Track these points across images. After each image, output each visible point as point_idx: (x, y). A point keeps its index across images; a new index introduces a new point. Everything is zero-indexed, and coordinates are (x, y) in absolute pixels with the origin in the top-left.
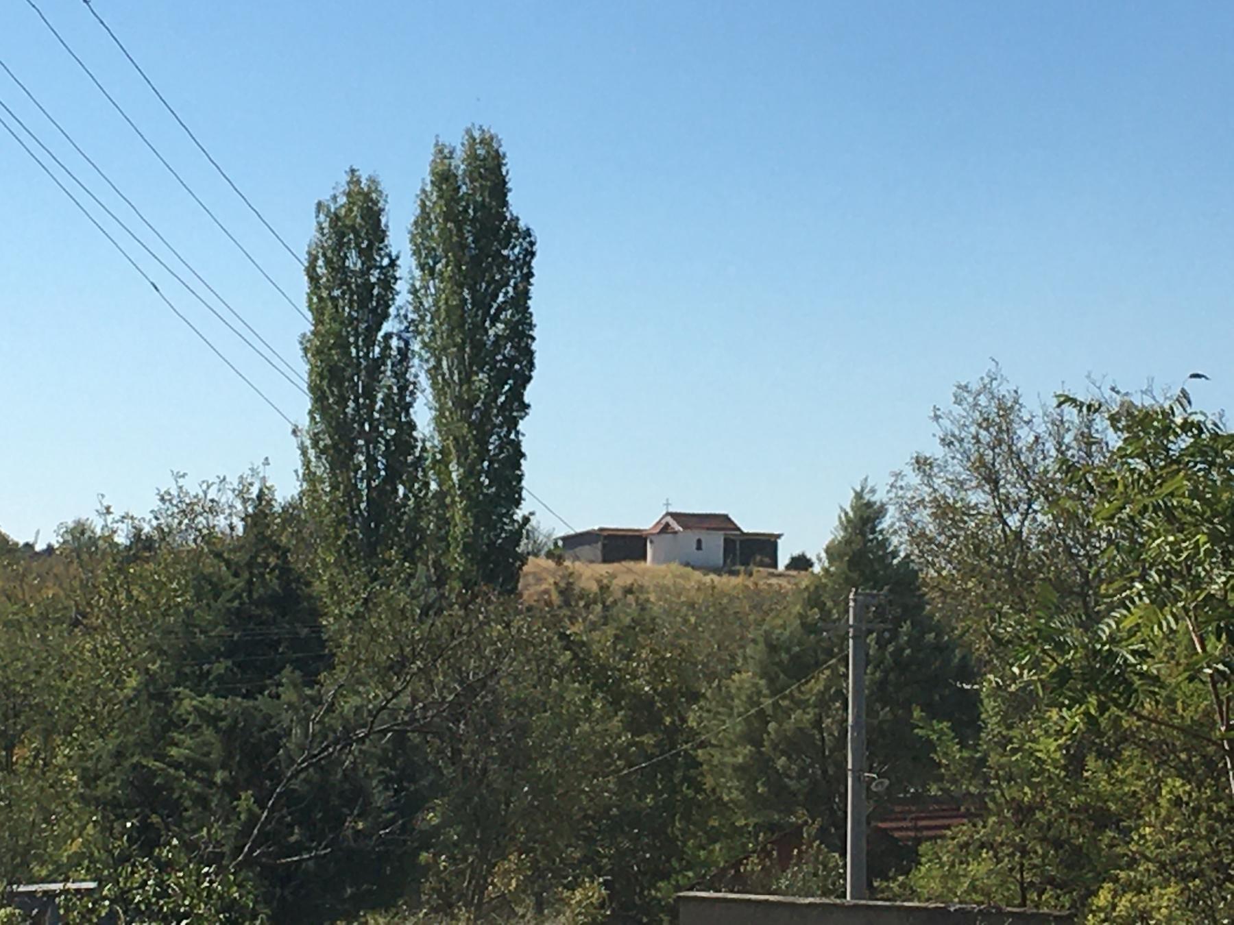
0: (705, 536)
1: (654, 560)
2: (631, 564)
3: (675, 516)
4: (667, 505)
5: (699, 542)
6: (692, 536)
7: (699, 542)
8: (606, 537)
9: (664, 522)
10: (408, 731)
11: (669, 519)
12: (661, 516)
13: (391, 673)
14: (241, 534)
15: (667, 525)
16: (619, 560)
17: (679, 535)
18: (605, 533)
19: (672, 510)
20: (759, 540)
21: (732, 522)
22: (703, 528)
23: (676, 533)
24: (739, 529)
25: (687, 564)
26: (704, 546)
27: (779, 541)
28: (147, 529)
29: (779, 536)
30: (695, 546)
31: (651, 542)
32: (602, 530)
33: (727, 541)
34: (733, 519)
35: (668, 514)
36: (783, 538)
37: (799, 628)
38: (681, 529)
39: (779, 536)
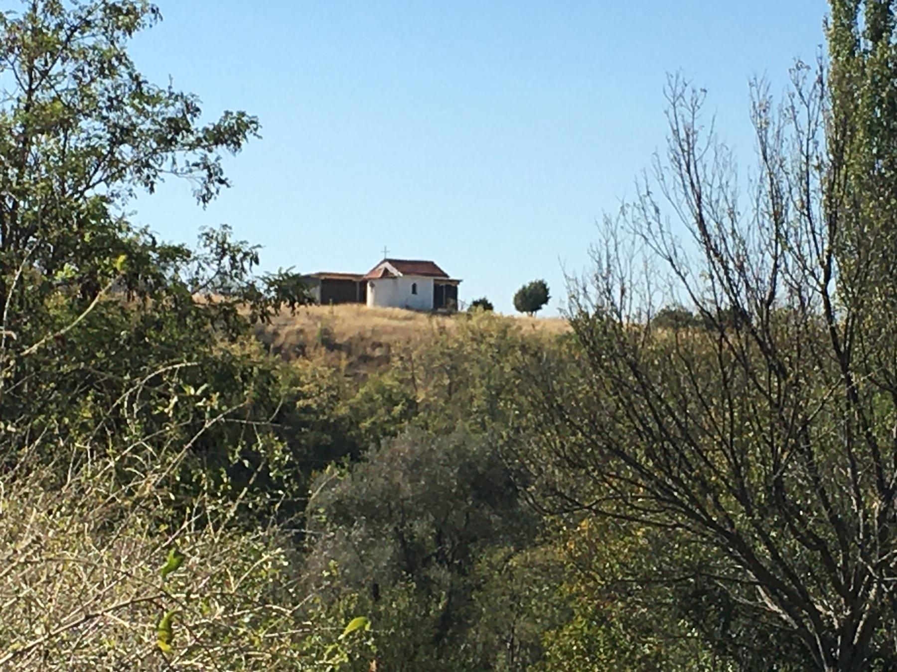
0: (419, 280)
1: (376, 302)
2: (355, 306)
3: (395, 263)
4: (385, 252)
5: (414, 286)
6: (410, 280)
7: (414, 286)
8: (323, 281)
9: (383, 266)
10: (465, 661)
11: (387, 265)
12: (378, 262)
13: (374, 520)
14: (282, 303)
15: (386, 271)
16: (336, 302)
17: (399, 280)
18: (323, 278)
19: (389, 257)
20: (350, 281)
21: (439, 269)
22: (419, 274)
23: (395, 278)
24: (446, 276)
25: (408, 308)
26: (418, 289)
27: (459, 287)
28: (544, 336)
29: (458, 282)
30: (411, 290)
31: (372, 286)
32: (321, 274)
33: (437, 288)
34: (439, 265)
35: (386, 260)
36: (461, 283)
37: (317, 334)
38: (401, 275)
39: (458, 282)
